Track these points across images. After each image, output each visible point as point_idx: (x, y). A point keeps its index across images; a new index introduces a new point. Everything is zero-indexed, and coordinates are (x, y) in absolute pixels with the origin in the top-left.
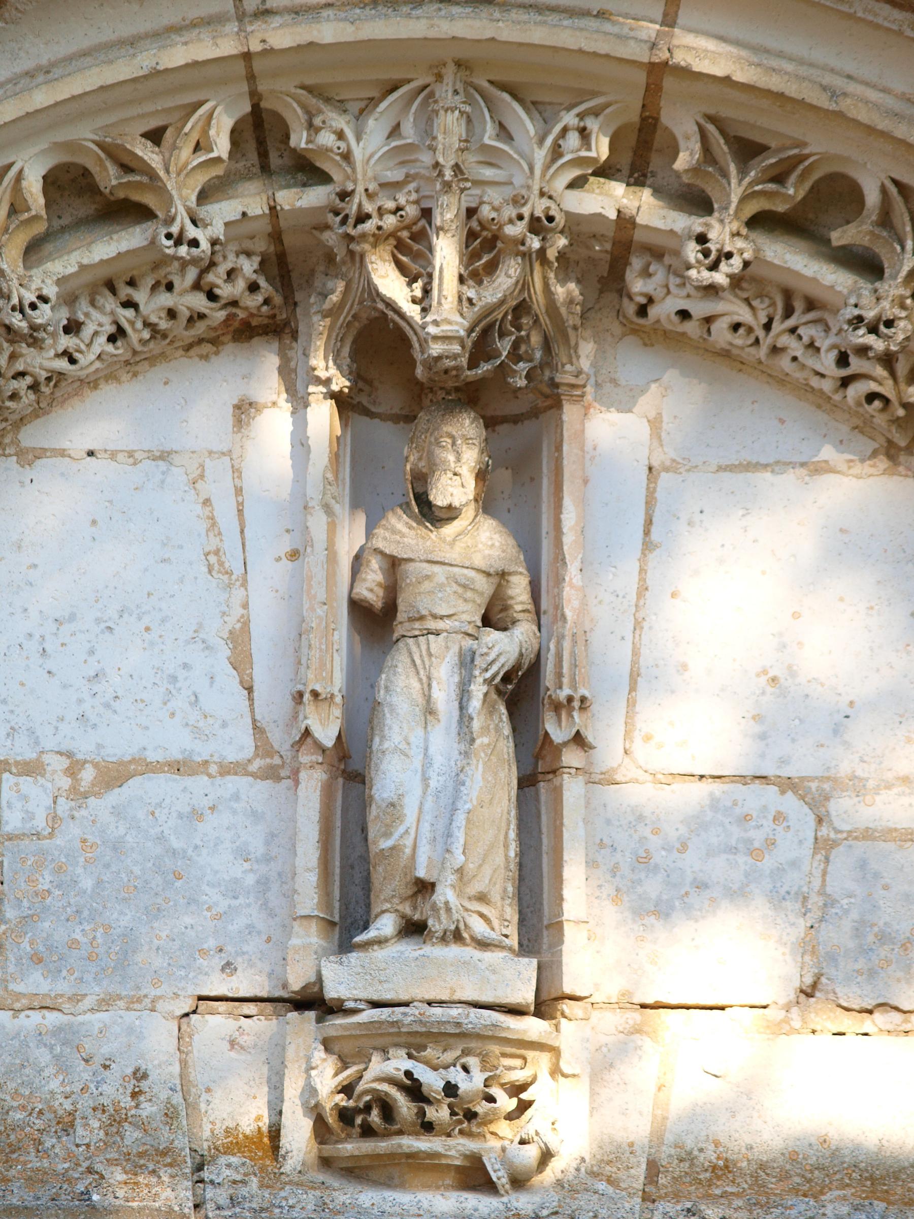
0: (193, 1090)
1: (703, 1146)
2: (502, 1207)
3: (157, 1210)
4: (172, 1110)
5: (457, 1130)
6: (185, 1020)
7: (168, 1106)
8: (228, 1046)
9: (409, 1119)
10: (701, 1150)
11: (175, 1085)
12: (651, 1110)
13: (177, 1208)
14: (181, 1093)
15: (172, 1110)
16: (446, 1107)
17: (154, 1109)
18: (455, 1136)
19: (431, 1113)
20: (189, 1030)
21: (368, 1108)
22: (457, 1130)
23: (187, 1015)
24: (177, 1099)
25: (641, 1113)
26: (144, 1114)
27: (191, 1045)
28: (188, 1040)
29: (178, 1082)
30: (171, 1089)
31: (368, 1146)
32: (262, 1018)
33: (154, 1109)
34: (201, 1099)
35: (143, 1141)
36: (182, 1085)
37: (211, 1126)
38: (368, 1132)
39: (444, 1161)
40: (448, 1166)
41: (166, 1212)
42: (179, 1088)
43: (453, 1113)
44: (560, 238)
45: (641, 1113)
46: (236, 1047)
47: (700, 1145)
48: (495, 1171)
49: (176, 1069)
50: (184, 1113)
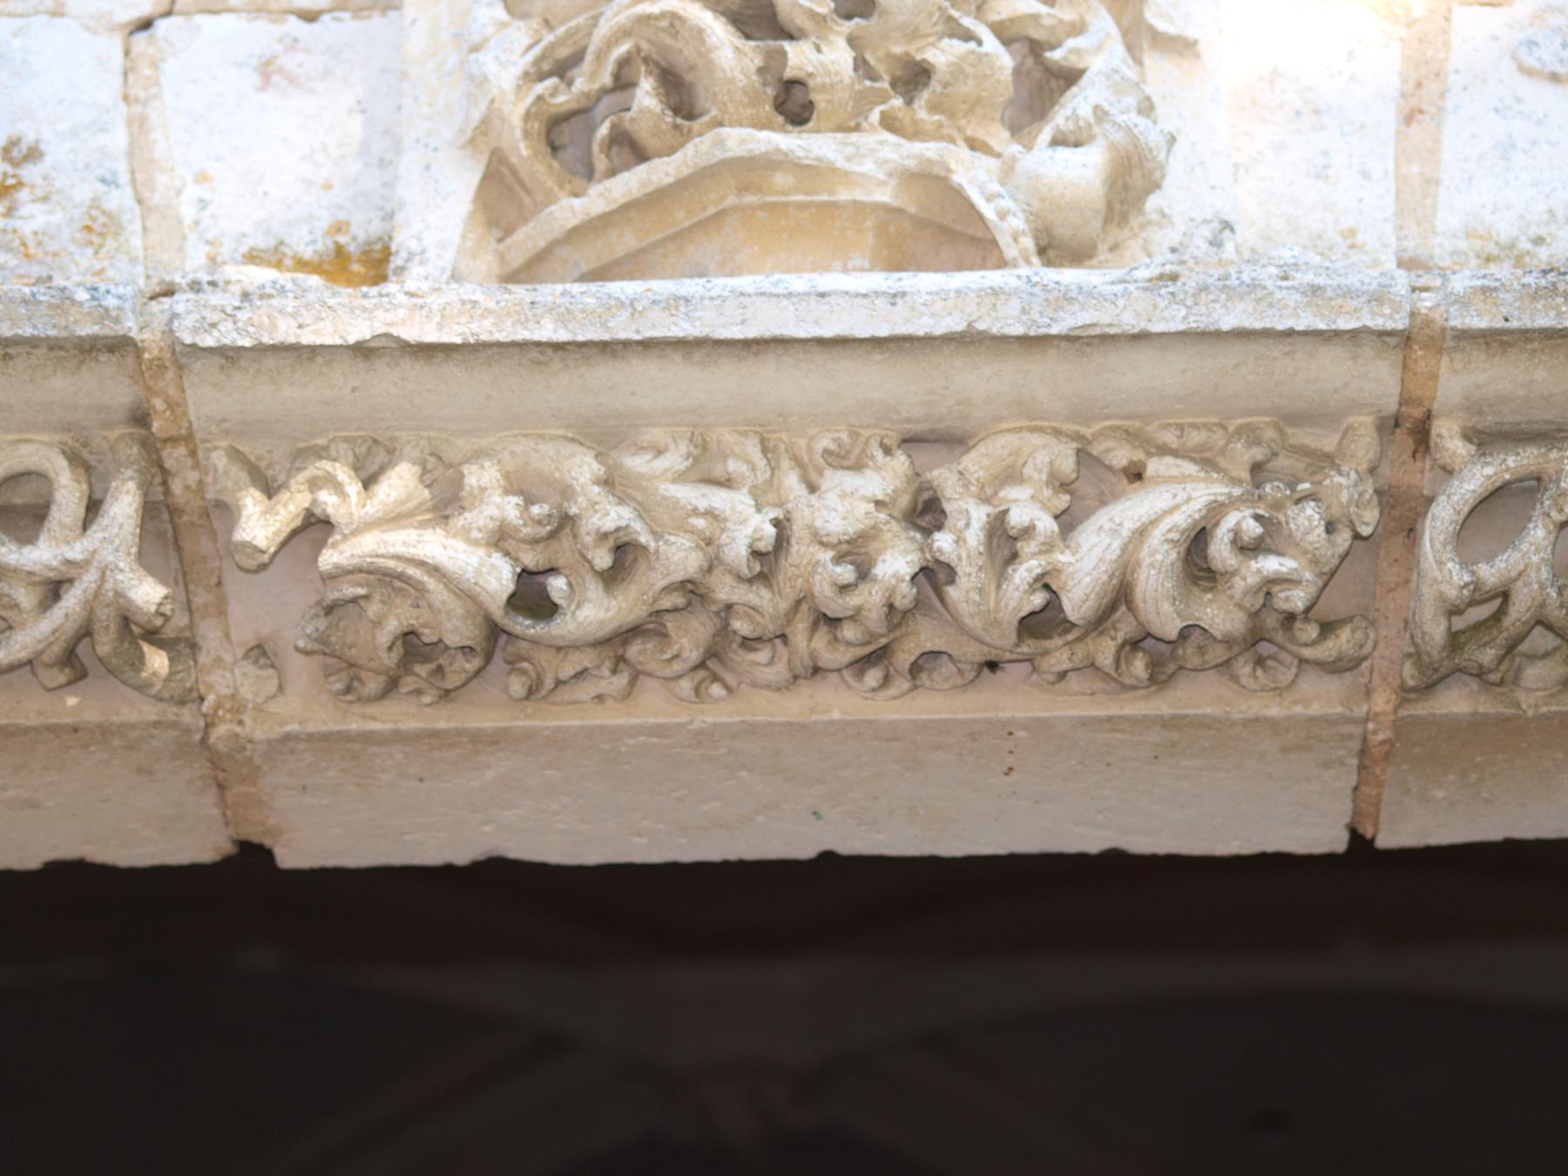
0: (162, 180)
1: (1543, 232)
2: (1021, 284)
3: (25, 301)
4: (103, 219)
5: (875, 116)
6: (141, 38)
7: (95, 213)
8: (255, 79)
9: (742, 80)
10: (1539, 241)
11: (114, 173)
12: (1391, 167)
13: (82, 295)
14: (129, 191)
15: (103, 219)
16: (841, 43)
17: (57, 218)
18: (872, 129)
19: (799, 57)
20: (151, 50)
21: (623, 83)
22: (875, 116)
23: (146, 25)
24: (120, 200)
25: (1366, 175)
26: (27, 228)
27: (157, 83)
28: (147, 71)
29: (122, 167)
30: (103, 181)
31: (631, 182)
32: (346, 16)
33: (57, 218)
34: (184, 197)
35: (22, 271)
36: (133, 173)
37: (208, 249)
38: (626, 147)
39: (843, 195)
40: (859, 207)
41: (51, 306)
42: (124, 178)
43: (861, 64)
44: (906, 552)
45: (1366, 175)
46: (275, 78)
47: (1534, 231)
48: (990, 198)
49: (118, 139)
50: (138, 226)
